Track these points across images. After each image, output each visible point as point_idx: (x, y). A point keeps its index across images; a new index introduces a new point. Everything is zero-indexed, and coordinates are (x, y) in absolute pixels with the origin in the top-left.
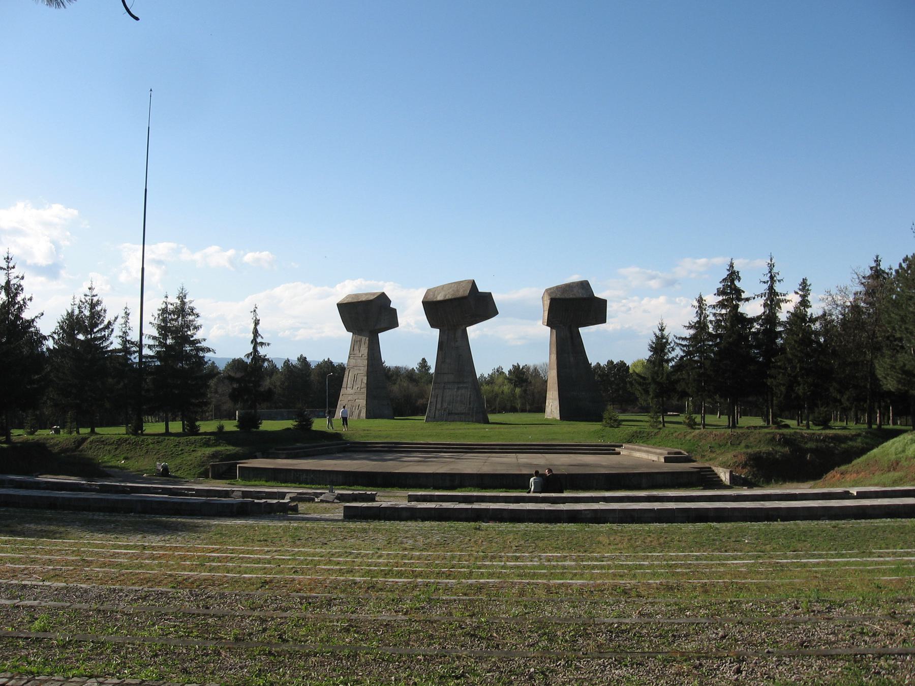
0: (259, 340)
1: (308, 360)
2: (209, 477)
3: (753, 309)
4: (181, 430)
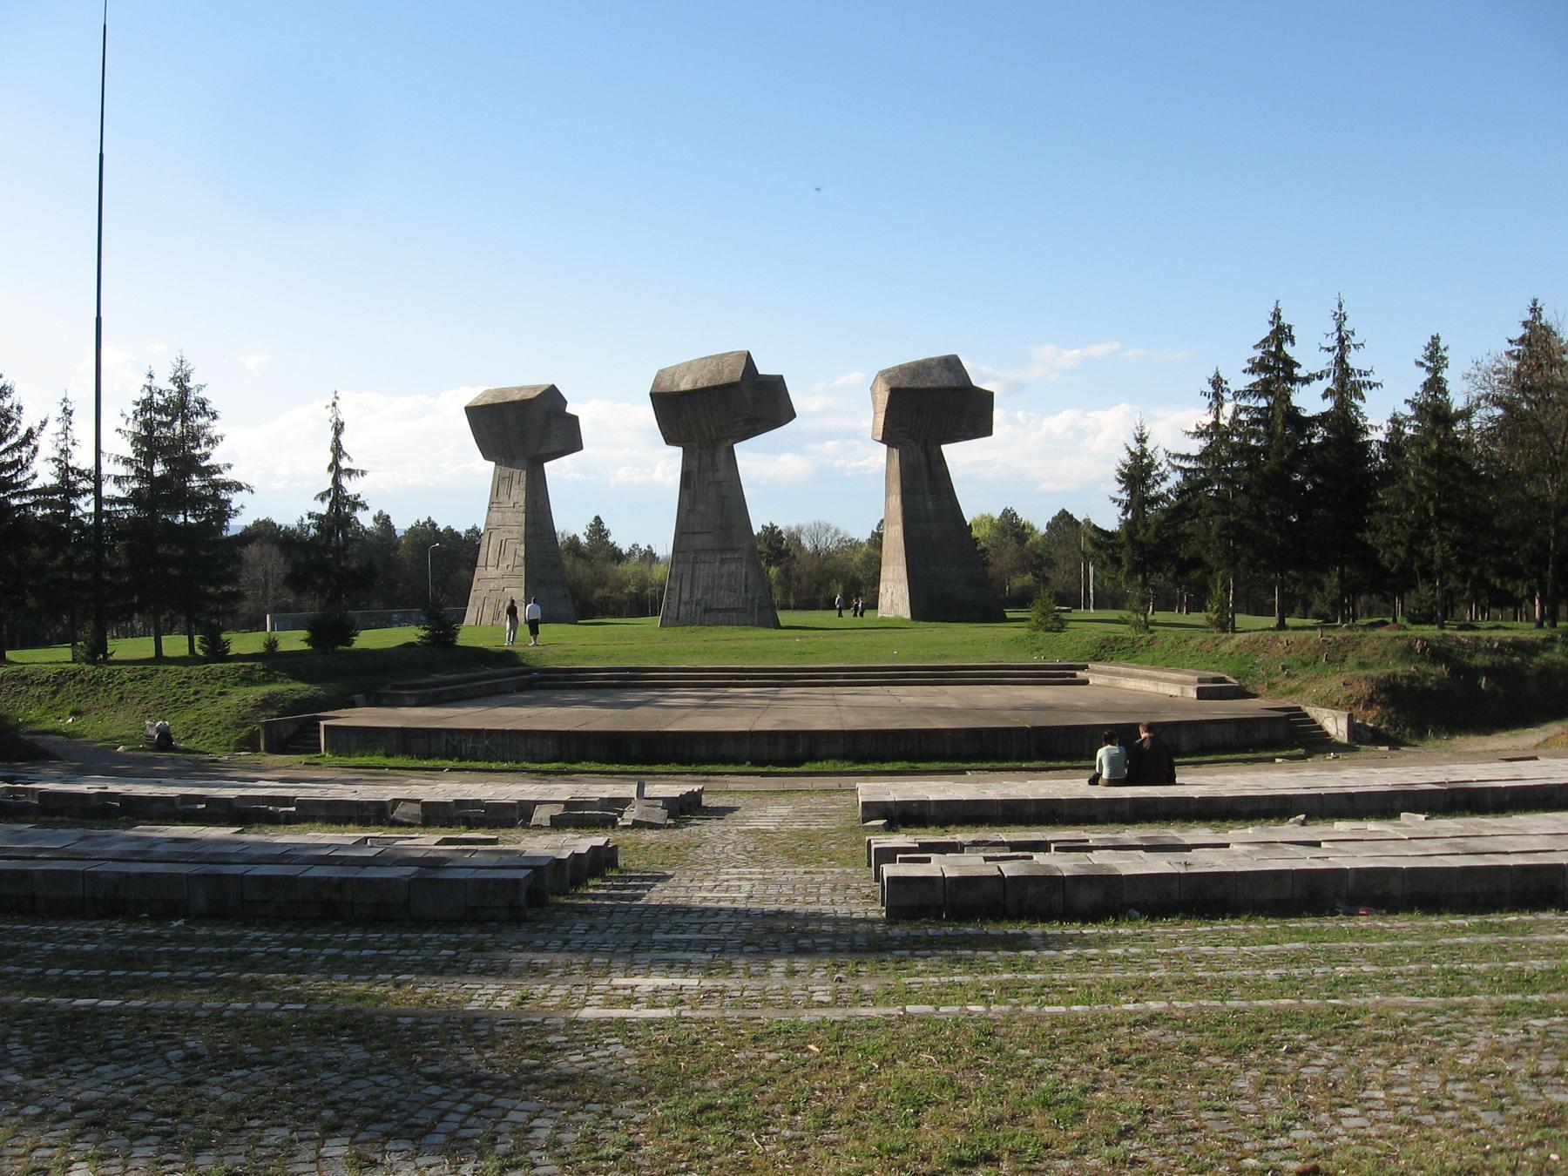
2: (260, 750)
3: (1310, 401)
4: (185, 651)
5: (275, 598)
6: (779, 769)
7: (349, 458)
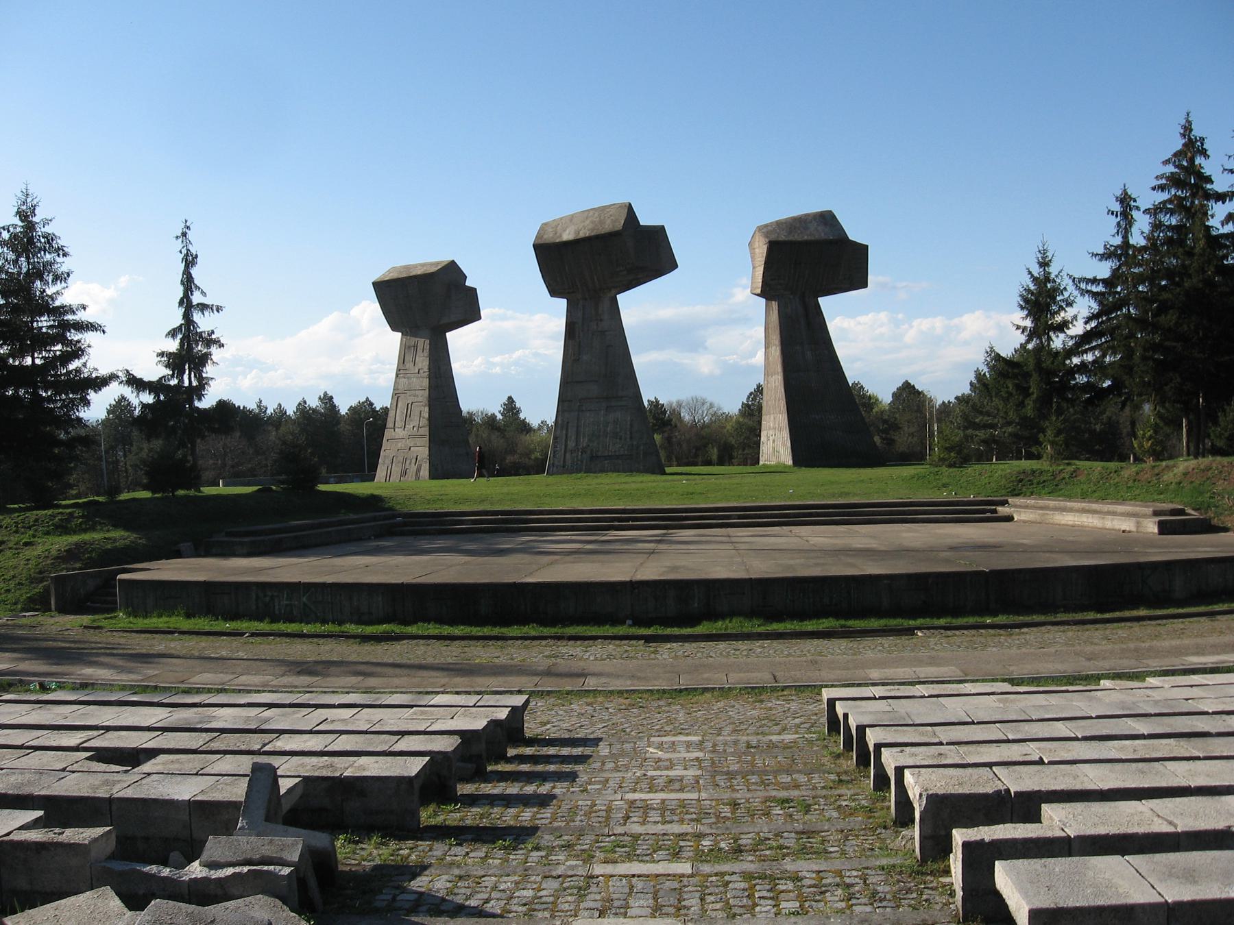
0: (196, 298)
1: (334, 400)
2: (50, 610)
5: (233, 467)
6: (668, 631)
7: (202, 292)
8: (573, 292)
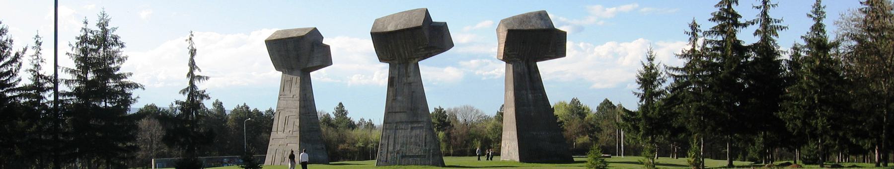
0: (196, 73)
1: (224, 105)
3: (747, 37)
5: (157, 150)
7: (199, 69)
8: (393, 60)
